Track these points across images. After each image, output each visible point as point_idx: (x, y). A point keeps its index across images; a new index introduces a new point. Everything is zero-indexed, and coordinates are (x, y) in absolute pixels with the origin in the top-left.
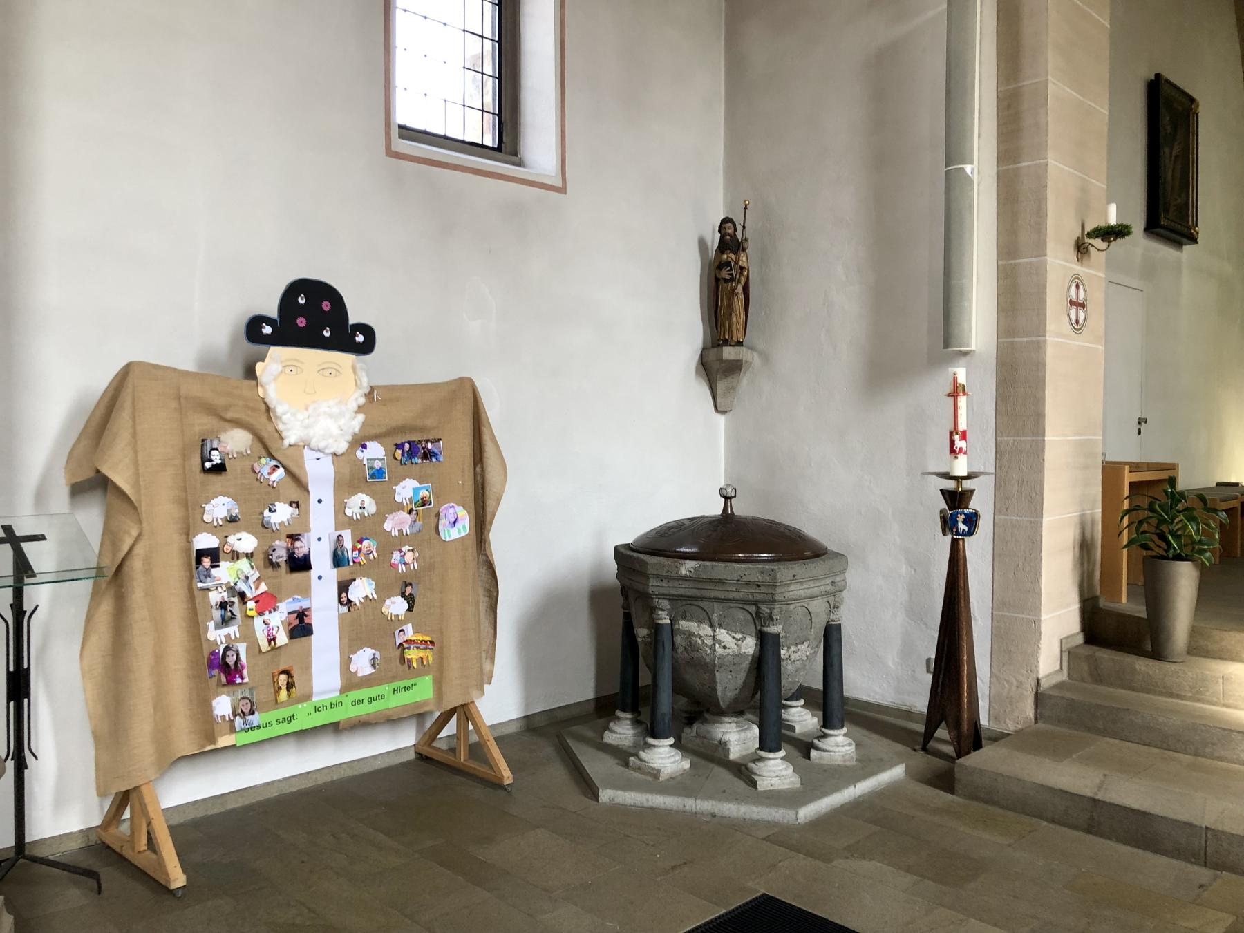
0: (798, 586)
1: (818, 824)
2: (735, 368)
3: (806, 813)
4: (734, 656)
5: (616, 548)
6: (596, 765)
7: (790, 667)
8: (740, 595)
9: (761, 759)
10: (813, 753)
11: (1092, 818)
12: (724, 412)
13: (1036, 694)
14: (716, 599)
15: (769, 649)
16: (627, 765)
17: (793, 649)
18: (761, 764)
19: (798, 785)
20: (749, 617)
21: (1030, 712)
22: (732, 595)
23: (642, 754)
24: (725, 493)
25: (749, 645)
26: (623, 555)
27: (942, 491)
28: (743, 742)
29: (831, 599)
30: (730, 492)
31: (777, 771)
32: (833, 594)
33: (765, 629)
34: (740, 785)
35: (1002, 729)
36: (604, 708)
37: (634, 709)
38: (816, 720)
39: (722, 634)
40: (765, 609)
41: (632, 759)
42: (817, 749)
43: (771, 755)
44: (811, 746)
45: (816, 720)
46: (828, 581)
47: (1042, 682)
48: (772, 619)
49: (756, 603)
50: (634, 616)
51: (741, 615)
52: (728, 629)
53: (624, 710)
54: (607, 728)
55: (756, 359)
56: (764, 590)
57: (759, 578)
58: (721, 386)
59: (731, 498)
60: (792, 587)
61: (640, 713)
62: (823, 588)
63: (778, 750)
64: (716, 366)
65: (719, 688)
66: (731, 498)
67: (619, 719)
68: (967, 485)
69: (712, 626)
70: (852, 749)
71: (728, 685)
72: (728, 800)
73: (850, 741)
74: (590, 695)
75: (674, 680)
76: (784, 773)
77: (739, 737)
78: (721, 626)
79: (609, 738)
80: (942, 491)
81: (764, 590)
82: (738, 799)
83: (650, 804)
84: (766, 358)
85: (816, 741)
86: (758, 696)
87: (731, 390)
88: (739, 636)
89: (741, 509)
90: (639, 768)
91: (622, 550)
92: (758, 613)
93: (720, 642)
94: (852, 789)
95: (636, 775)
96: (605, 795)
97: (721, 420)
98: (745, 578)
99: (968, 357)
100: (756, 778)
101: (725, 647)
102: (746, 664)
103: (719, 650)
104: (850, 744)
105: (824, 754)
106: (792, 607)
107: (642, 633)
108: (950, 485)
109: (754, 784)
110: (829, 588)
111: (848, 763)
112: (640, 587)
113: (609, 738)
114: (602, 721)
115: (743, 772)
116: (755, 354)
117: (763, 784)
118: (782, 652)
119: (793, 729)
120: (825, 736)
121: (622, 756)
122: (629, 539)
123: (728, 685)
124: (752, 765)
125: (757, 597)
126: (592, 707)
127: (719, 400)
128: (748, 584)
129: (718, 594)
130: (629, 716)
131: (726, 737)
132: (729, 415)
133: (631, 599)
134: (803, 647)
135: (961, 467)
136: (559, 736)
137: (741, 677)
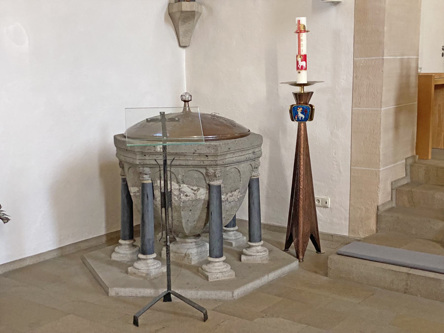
0: (231, 155)
1: (245, 298)
2: (191, 16)
3: (238, 292)
4: (192, 201)
5: (115, 137)
6: (105, 274)
7: (227, 206)
8: (196, 163)
9: (209, 262)
10: (243, 258)
11: (407, 285)
12: (184, 47)
13: (377, 214)
14: (180, 165)
15: (214, 194)
16: (127, 272)
17: (230, 194)
18: (210, 266)
19: (234, 277)
20: (201, 176)
21: (373, 226)
22: (190, 163)
23: (136, 265)
24: (184, 97)
25: (203, 194)
26: (119, 141)
27: (312, 93)
28: (199, 254)
29: (253, 163)
30: (187, 97)
31: (219, 269)
32: (254, 160)
33: (212, 183)
34: (199, 280)
35: (357, 236)
36: (112, 239)
37: (131, 237)
38: (245, 238)
39: (185, 187)
40: (211, 170)
41: (130, 269)
42: (246, 255)
43: (217, 260)
44: (241, 254)
45: (245, 238)
46: (251, 151)
47: (380, 208)
48: (215, 176)
49: (205, 167)
50: (128, 179)
51: (196, 175)
52: (189, 184)
53: (124, 239)
54: (113, 251)
55: (204, 10)
56: (210, 158)
57: (205, 151)
58: (182, 29)
59: (188, 101)
60: (228, 156)
61: (135, 241)
62: (247, 156)
63: (221, 256)
64: (178, 15)
65: (183, 221)
66: (188, 101)
67: (121, 245)
68: (307, 89)
69: (178, 183)
70: (267, 253)
71: (189, 219)
72: (191, 288)
73: (266, 249)
74: (103, 232)
75: (155, 218)
76: (225, 270)
77: (193, 251)
78: (183, 183)
79: (115, 257)
80: (312, 93)
81: (210, 158)
82: (196, 287)
83: (142, 294)
84: (210, 10)
85: (244, 250)
86: (208, 224)
87: (189, 32)
88: (195, 188)
89: (198, 108)
90: (135, 274)
91: (119, 138)
92: (207, 173)
93: (184, 192)
94: (266, 277)
95: (132, 277)
96: (112, 292)
97: (183, 51)
98: (198, 151)
99: (338, 6)
100: (208, 274)
101: (186, 196)
102: (200, 205)
103: (183, 198)
104: (265, 251)
105: (250, 257)
106: (228, 168)
107: (133, 190)
108: (298, 90)
109: (207, 278)
110: (251, 156)
111: (265, 262)
112: (131, 161)
113: (115, 257)
114: (111, 247)
115: (199, 271)
116: (203, 7)
117: (212, 278)
118: (223, 197)
119: (231, 244)
120: (250, 247)
121: (124, 267)
122: (123, 131)
123: (189, 219)
124: (204, 267)
125: (206, 163)
126: (104, 240)
127: (181, 38)
128: (200, 155)
129: (183, 163)
130: (127, 242)
131: (190, 251)
132: (187, 48)
133: (126, 169)
134: (235, 193)
135: (303, 78)
136: (83, 259)
137: (197, 214)
